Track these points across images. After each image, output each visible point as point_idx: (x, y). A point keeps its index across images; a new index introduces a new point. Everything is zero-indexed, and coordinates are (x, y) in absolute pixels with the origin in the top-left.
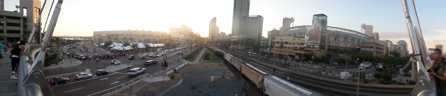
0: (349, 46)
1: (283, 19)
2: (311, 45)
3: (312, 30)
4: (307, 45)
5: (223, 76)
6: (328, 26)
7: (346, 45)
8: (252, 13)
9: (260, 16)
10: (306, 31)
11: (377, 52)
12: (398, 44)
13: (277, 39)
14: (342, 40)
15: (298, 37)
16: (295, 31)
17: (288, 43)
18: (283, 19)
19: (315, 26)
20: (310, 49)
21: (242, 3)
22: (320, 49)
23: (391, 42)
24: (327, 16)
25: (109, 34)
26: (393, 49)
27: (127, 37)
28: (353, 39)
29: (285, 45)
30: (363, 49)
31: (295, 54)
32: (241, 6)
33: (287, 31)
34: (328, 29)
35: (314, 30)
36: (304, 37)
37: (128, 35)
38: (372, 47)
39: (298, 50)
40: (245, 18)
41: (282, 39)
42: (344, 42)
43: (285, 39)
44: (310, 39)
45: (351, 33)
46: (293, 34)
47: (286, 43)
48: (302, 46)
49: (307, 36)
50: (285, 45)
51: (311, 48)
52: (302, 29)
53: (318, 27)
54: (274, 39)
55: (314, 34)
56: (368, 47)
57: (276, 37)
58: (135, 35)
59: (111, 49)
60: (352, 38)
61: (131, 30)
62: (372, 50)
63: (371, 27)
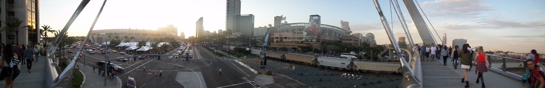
0: (333, 39)
1: (466, 39)
2: (308, 40)
3: (309, 28)
4: (305, 39)
5: (456, 68)
6: (321, 23)
7: (331, 38)
8: (244, 12)
9: (252, 15)
10: (304, 28)
11: (354, 44)
12: (366, 36)
13: (276, 35)
14: (327, 34)
15: (297, 33)
16: (294, 27)
17: (288, 38)
18: (275, 17)
19: (312, 24)
20: (308, 42)
21: (234, 3)
22: (317, 42)
23: (361, 34)
24: (320, 16)
25: (108, 32)
26: (363, 41)
27: (128, 36)
28: (335, 34)
29: (284, 40)
30: (344, 42)
31: (297, 47)
32: (234, 6)
33: (279, 28)
34: (321, 26)
35: (312, 27)
36: (303, 33)
37: (129, 34)
38: (351, 40)
39: (300, 43)
40: (237, 17)
41: (281, 35)
42: (329, 36)
43: (285, 35)
44: (308, 35)
45: (328, 27)
46: (291, 30)
47: (286, 38)
48: (302, 40)
49: (305, 32)
50: (284, 40)
51: (309, 41)
52: (289, 26)
53: (315, 26)
54: (273, 35)
55: (311, 30)
56: (348, 40)
57: (275, 34)
58: (136, 34)
59: (126, 49)
60: (329, 31)
61: (132, 28)
62: (351, 42)
63: (347, 23)
